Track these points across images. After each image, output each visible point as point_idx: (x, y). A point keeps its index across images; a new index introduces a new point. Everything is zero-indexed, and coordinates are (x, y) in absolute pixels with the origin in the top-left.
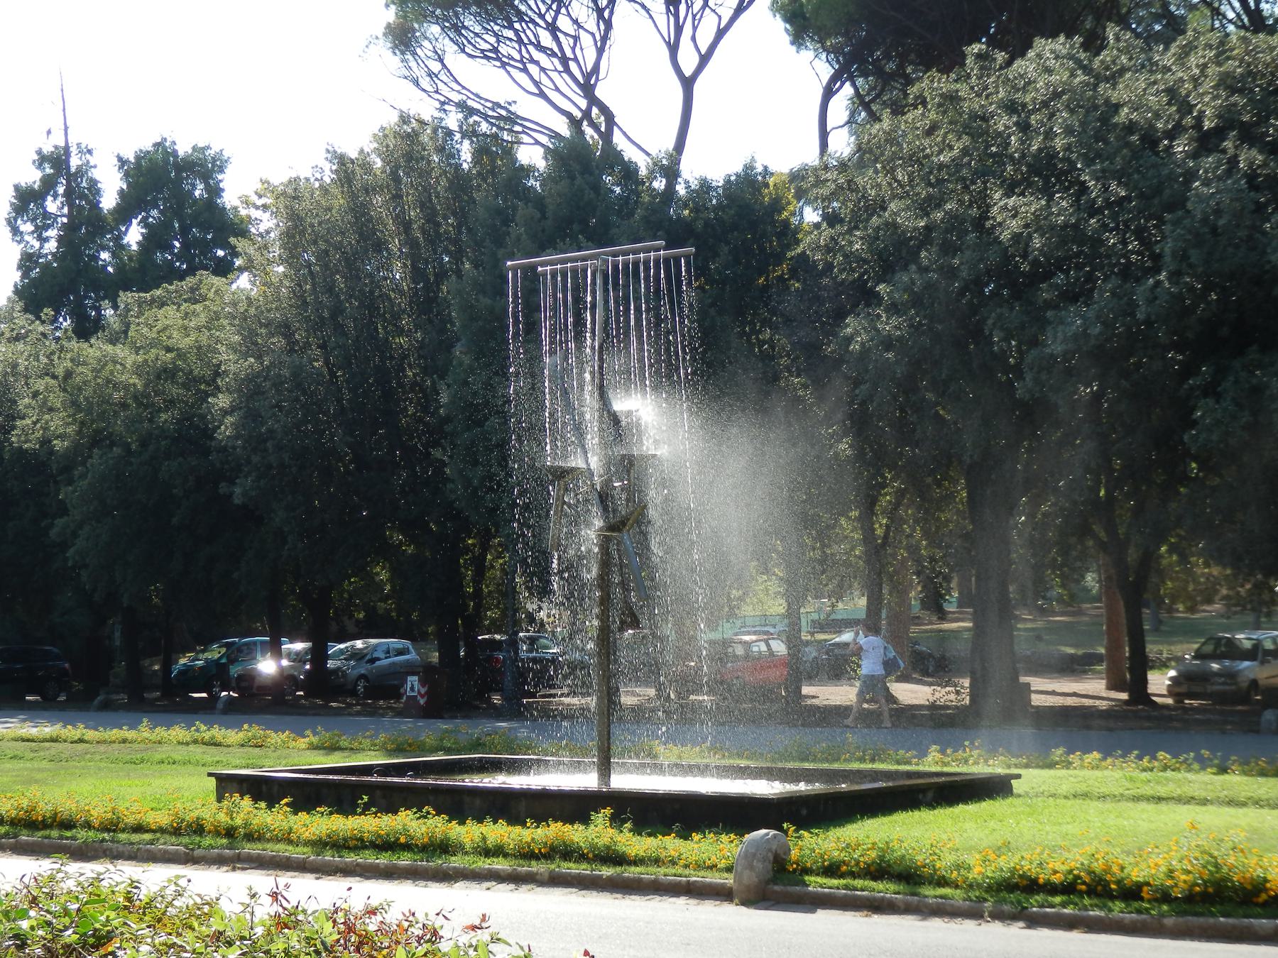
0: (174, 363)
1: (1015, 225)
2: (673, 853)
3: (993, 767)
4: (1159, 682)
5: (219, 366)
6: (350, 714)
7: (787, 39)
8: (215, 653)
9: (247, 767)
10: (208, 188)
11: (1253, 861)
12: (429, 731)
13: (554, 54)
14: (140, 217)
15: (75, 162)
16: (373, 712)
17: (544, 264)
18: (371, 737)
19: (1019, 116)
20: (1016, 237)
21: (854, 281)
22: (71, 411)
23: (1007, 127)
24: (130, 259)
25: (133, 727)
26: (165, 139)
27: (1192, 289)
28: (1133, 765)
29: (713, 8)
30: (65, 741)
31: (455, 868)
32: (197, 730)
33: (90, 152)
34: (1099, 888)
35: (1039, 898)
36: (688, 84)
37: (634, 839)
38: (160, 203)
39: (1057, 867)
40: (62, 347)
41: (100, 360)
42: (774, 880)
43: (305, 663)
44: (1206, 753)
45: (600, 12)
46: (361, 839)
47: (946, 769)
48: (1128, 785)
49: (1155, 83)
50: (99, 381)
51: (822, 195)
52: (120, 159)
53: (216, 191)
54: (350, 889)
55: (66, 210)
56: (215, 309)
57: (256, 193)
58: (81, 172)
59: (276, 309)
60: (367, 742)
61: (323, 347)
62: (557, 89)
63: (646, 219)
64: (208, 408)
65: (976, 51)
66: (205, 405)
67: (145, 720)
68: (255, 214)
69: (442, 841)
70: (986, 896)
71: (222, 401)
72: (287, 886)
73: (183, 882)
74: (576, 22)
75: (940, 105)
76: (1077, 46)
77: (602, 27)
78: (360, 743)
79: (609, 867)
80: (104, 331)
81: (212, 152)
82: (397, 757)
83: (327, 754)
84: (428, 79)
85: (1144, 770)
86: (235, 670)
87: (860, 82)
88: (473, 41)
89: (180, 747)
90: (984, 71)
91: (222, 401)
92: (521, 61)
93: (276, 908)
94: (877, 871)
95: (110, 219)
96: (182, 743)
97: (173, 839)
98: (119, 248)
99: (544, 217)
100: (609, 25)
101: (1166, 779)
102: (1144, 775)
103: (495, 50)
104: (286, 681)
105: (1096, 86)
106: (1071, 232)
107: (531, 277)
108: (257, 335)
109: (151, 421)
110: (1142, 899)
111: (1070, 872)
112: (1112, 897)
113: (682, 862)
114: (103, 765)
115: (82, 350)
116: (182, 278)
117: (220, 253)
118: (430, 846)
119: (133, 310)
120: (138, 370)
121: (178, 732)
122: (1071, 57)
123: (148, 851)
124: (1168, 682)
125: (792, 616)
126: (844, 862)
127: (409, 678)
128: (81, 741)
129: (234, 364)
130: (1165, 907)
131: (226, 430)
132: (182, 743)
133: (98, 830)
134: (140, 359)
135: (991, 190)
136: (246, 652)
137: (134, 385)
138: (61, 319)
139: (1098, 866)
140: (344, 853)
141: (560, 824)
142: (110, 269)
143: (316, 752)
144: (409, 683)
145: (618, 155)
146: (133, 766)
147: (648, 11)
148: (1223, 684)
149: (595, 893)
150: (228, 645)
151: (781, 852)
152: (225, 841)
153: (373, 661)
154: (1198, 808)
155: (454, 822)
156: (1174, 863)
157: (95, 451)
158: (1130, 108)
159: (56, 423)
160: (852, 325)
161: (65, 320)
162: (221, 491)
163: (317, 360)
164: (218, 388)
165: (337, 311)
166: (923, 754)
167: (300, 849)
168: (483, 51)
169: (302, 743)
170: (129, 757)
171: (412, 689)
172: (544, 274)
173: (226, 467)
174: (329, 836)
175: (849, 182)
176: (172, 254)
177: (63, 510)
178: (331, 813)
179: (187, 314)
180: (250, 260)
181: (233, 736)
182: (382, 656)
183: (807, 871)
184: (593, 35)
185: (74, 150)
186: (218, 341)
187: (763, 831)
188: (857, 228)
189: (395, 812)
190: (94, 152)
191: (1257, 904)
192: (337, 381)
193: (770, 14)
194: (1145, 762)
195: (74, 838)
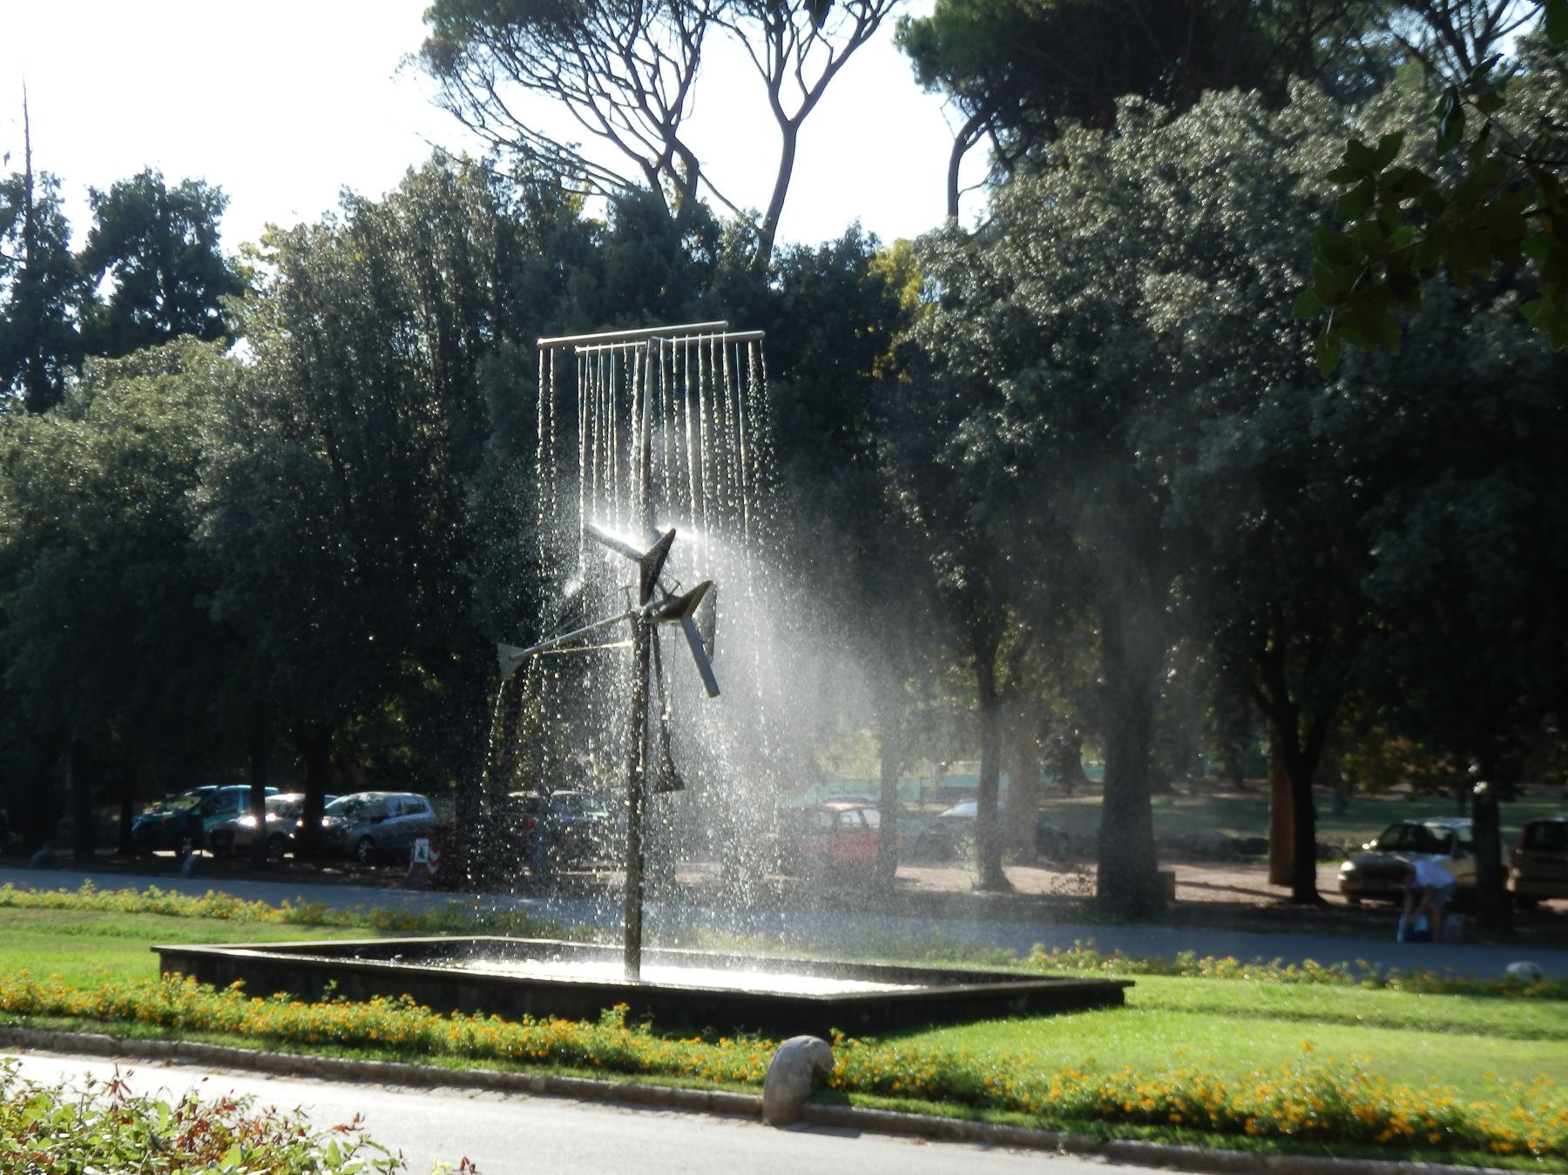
1: (1168, 311)
2: (694, 1061)
3: (1110, 972)
4: (1332, 877)
5: (198, 452)
6: (344, 883)
8: (187, 802)
9: (207, 942)
10: (201, 233)
11: (1377, 1091)
13: (628, 86)
14: (115, 265)
15: (38, 194)
16: (373, 882)
17: (583, 343)
18: (360, 911)
19: (1179, 183)
22: (16, 501)
23: (1163, 197)
24: (101, 315)
25: (73, 888)
26: (150, 172)
27: (1376, 401)
28: (1275, 975)
29: (824, 37)
31: (433, 1071)
32: (151, 896)
33: (57, 183)
34: (1196, 1118)
35: (1124, 1128)
36: (790, 129)
37: (652, 1043)
38: (141, 248)
39: (1147, 1092)
40: (10, 421)
41: (54, 440)
42: (812, 1098)
43: (296, 819)
44: (1362, 963)
45: (686, 37)
46: (324, 1033)
47: (1050, 973)
48: (1264, 997)
51: (937, 271)
52: (93, 192)
53: (209, 237)
54: (206, 1079)
55: (24, 253)
56: (198, 382)
57: (262, 241)
58: (44, 207)
59: (273, 384)
60: (356, 918)
61: (328, 433)
62: (631, 129)
65: (1129, 104)
66: (179, 500)
67: (88, 881)
68: (260, 266)
70: (1060, 1123)
71: (200, 495)
72: (130, 1074)
73: (13, 1066)
74: (655, 48)
75: (1083, 167)
76: (1253, 102)
77: (688, 55)
81: (207, 189)
82: (391, 936)
83: (307, 930)
85: (1288, 981)
86: (210, 825)
88: (529, 66)
89: (128, 916)
91: (200, 495)
92: (587, 93)
95: (78, 266)
97: (98, 1026)
98: (88, 302)
99: (602, 284)
100: (696, 52)
101: (1313, 993)
102: (1290, 988)
103: (556, 78)
104: (267, 839)
105: (1272, 151)
106: (1233, 327)
107: (567, 358)
108: (247, 415)
109: (114, 515)
111: (1163, 1098)
112: (1210, 1130)
113: (705, 1072)
114: (31, 934)
115: (33, 425)
116: (162, 342)
117: (212, 313)
119: (100, 379)
120: (102, 452)
121: (127, 898)
122: (1244, 115)
123: (67, 1039)
124: (1342, 877)
126: (897, 1079)
127: (418, 841)
129: (217, 451)
130: (1270, 1144)
131: (204, 530)
133: (8, 1012)
134: (103, 440)
135: (1142, 272)
136: (224, 803)
137: (95, 471)
138: (14, 387)
139: (1196, 1092)
140: (303, 1048)
142: (77, 327)
143: (292, 927)
144: (418, 848)
145: (703, 210)
146: (68, 937)
147: (743, 37)
149: (599, 1107)
151: (822, 1064)
152: (159, 1030)
154: (1346, 1029)
155: (438, 1016)
156: (1284, 1091)
157: (45, 550)
160: (966, 430)
161: (19, 388)
164: (197, 479)
165: (347, 390)
166: (1023, 953)
167: (251, 1042)
168: (540, 79)
169: (277, 915)
170: (64, 926)
171: (421, 854)
172: (583, 355)
175: (972, 256)
176: (153, 311)
178: (291, 1000)
181: (193, 904)
183: (853, 1088)
185: (37, 179)
186: (200, 421)
188: (978, 313)
189: (367, 1000)
190: (62, 184)
191: (1378, 1144)
193: (894, 49)
194: (1290, 971)
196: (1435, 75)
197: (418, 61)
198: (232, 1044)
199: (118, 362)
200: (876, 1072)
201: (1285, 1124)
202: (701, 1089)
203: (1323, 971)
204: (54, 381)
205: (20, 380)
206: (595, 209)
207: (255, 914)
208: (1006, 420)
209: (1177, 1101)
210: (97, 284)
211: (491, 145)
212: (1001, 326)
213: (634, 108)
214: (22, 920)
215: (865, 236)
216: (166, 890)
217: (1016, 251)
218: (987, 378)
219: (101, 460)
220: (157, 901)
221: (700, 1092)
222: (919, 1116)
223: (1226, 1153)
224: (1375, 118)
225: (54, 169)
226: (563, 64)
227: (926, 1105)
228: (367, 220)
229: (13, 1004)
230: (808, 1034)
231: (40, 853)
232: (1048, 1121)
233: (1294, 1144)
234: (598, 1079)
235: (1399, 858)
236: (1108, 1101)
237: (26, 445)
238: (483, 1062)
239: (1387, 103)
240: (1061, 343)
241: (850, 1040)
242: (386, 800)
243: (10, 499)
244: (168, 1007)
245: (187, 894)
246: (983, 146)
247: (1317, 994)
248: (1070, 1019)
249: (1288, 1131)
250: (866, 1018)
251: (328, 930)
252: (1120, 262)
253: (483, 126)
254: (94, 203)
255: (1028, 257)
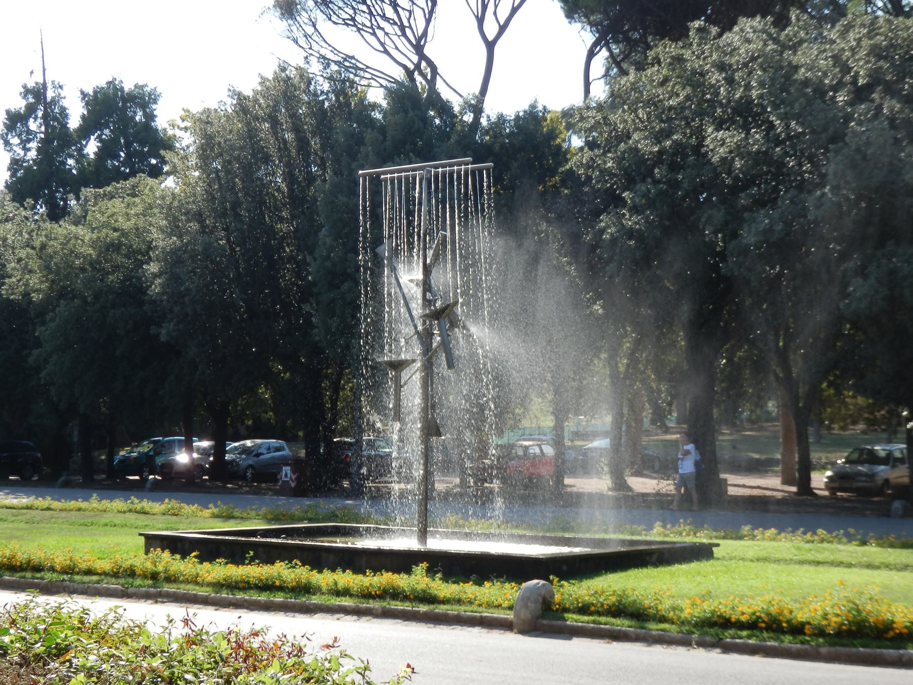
0: (119, 240)
2: (470, 596)
3: (702, 538)
4: (819, 480)
5: (151, 242)
6: (241, 493)
7: (561, 14)
8: (145, 447)
9: (167, 529)
10: (145, 115)
11: (884, 608)
12: (297, 506)
13: (395, 23)
15: (50, 94)
16: (257, 492)
18: (256, 509)
19: (727, 73)
20: (723, 160)
21: (608, 189)
22: (45, 273)
23: (718, 81)
24: (89, 164)
25: (86, 499)
26: (115, 79)
27: (847, 199)
28: (800, 539)
30: (37, 509)
31: (314, 604)
32: (132, 503)
33: (61, 87)
34: (775, 626)
35: (732, 632)
36: (490, 46)
37: (443, 585)
38: (111, 125)
39: (745, 610)
42: (543, 616)
43: (209, 456)
44: (852, 531)
46: (248, 582)
47: (667, 539)
48: (796, 552)
49: (825, 51)
50: (65, 251)
51: (585, 127)
52: (82, 92)
53: (150, 117)
55: (43, 129)
57: (181, 118)
58: (54, 102)
59: (193, 202)
60: (253, 513)
62: (397, 48)
63: (458, 142)
64: (143, 272)
65: (697, 26)
67: (95, 495)
68: (179, 133)
69: (306, 585)
71: (153, 268)
72: (195, 615)
73: (120, 611)
75: (670, 64)
76: (769, 23)
78: (248, 514)
79: (424, 605)
80: (69, 216)
82: (274, 524)
83: (225, 521)
84: (304, 39)
85: (808, 542)
86: (159, 460)
87: (614, 47)
89: (119, 515)
90: (703, 40)
91: (153, 268)
92: (371, 28)
93: (187, 630)
94: (616, 611)
95: (75, 135)
96: (121, 512)
97: (114, 580)
101: (824, 549)
103: (353, 19)
104: (196, 468)
105: (782, 53)
107: (376, 182)
108: (179, 220)
109: (102, 280)
110: (805, 634)
111: (754, 613)
114: (64, 526)
117: (153, 161)
118: (297, 588)
119: (90, 201)
120: (94, 244)
121: (118, 504)
122: (764, 31)
123: (96, 588)
124: (826, 480)
125: (559, 428)
126: (593, 604)
127: (284, 468)
128: (48, 509)
129: (162, 241)
130: (821, 640)
131: (156, 288)
132: (121, 512)
135: (706, 126)
137: (90, 255)
138: (38, 207)
139: (774, 610)
140: (236, 592)
141: (390, 574)
142: (74, 172)
143: (216, 520)
144: (284, 473)
146: (85, 527)
148: (865, 481)
149: (414, 623)
150: (155, 442)
151: (548, 597)
152: (150, 582)
153: (258, 455)
154: (846, 570)
155: (315, 571)
156: (827, 609)
157: (62, 301)
158: (806, 69)
159: (34, 281)
160: (604, 220)
161: (41, 207)
162: (151, 332)
163: (221, 240)
164: (150, 258)
165: (236, 205)
166: (650, 528)
167: (204, 589)
168: (344, 20)
169: (207, 513)
170: (82, 521)
171: (286, 476)
172: (386, 180)
173: (155, 315)
174: (225, 580)
175: (605, 118)
177: (38, 343)
178: (227, 563)
179: (129, 204)
180: (175, 167)
181: (157, 507)
182: (265, 451)
183: (566, 610)
184: (423, 10)
185: (49, 85)
187: (535, 581)
188: (609, 151)
190: (64, 87)
191: (887, 639)
192: (236, 255)
194: (808, 536)
195: (42, 578)
196: (872, 5)
197: (272, 11)
198: (194, 590)
199: (101, 191)
200: (580, 600)
201: (829, 628)
202: (476, 612)
203: (829, 535)
204: (62, 203)
205: (42, 202)
206: (376, 96)
207: (194, 512)
208: (628, 214)
209: (763, 615)
210: (85, 146)
211: (317, 60)
212: (624, 159)
213: (399, 36)
214: (58, 518)
215: (540, 108)
216: (141, 499)
217: (631, 114)
218: (616, 190)
219: (94, 248)
220: (136, 506)
221: (475, 614)
222: (607, 627)
223: (794, 646)
224: (843, 31)
225: (59, 80)
226: (357, 11)
227: (613, 620)
228: (243, 105)
229: (62, 568)
230: (538, 579)
231: (62, 479)
232: (685, 628)
233: (836, 640)
234: (413, 607)
235: (860, 468)
236: (720, 617)
237: (50, 240)
238: (344, 599)
239: (849, 23)
240: (659, 168)
241: (563, 582)
242: (262, 444)
243: (41, 272)
244: (154, 568)
245: (153, 501)
246: (602, 57)
247: (827, 549)
248: (684, 567)
249: (831, 632)
250: (565, 568)
251: (238, 521)
252: (693, 120)
253: (310, 48)
254: (83, 99)
255: (638, 118)
